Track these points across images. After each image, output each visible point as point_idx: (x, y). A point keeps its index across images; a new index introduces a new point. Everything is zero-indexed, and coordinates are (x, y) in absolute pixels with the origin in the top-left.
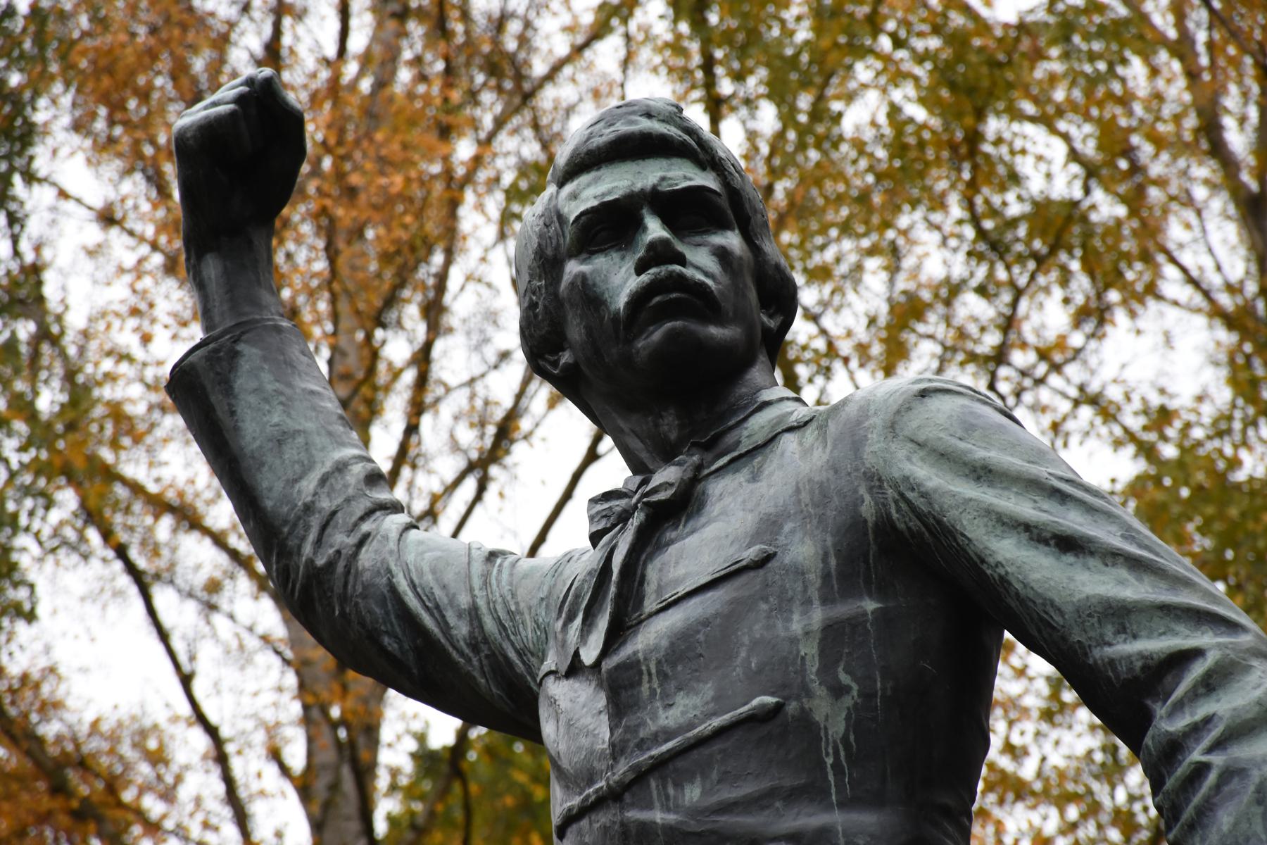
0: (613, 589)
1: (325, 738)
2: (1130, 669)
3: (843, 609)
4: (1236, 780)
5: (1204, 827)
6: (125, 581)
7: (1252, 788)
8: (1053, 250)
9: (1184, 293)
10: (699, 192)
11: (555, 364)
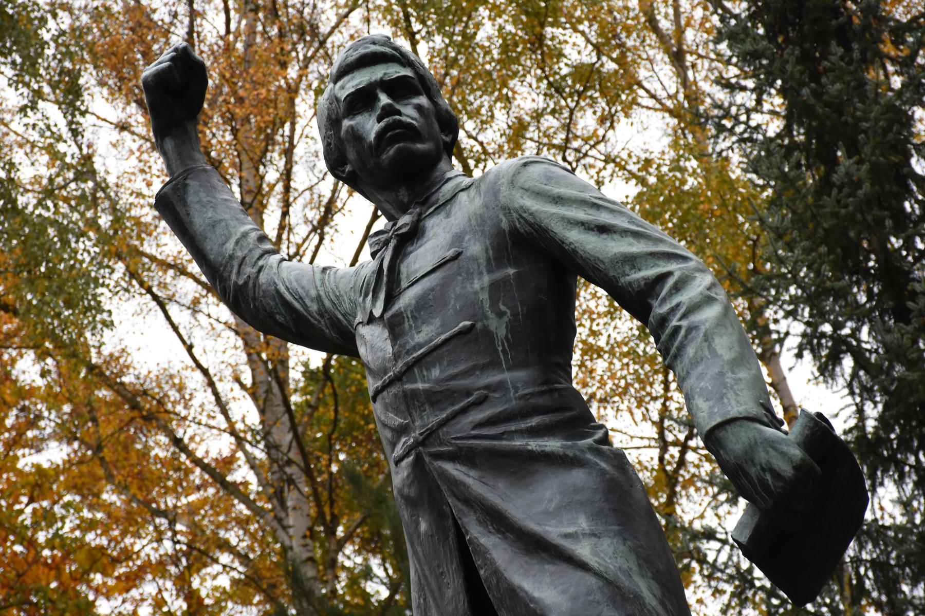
0: (385, 279)
1: (261, 368)
2: (639, 286)
3: (498, 275)
4: (694, 332)
5: (681, 356)
6: (153, 304)
7: (702, 334)
8: (586, 89)
9: (651, 102)
10: (405, 77)
11: (343, 172)
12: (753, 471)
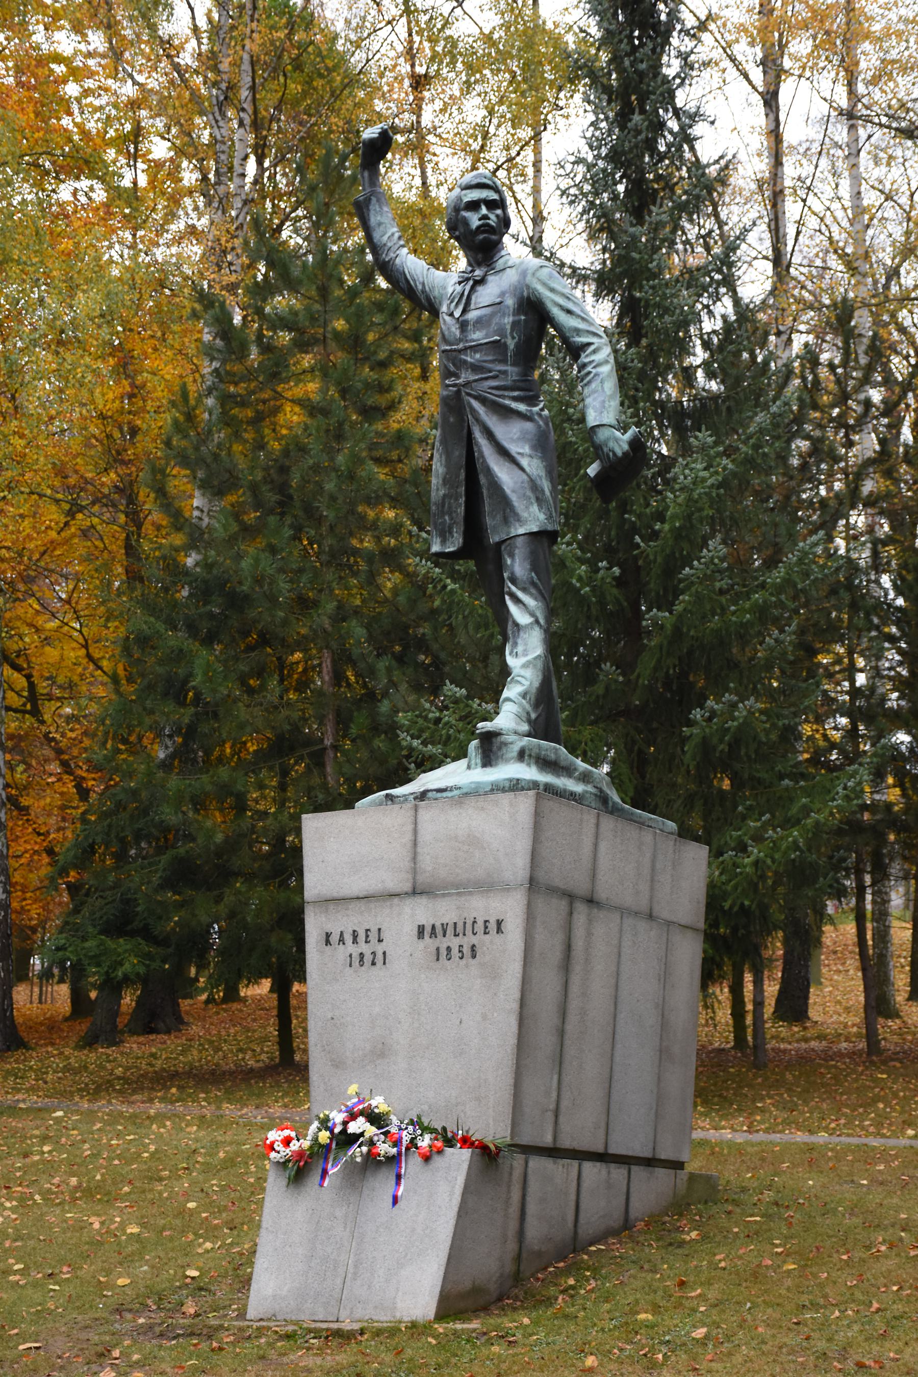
3: (517, 318)
10: (494, 200)
12: (605, 450)
